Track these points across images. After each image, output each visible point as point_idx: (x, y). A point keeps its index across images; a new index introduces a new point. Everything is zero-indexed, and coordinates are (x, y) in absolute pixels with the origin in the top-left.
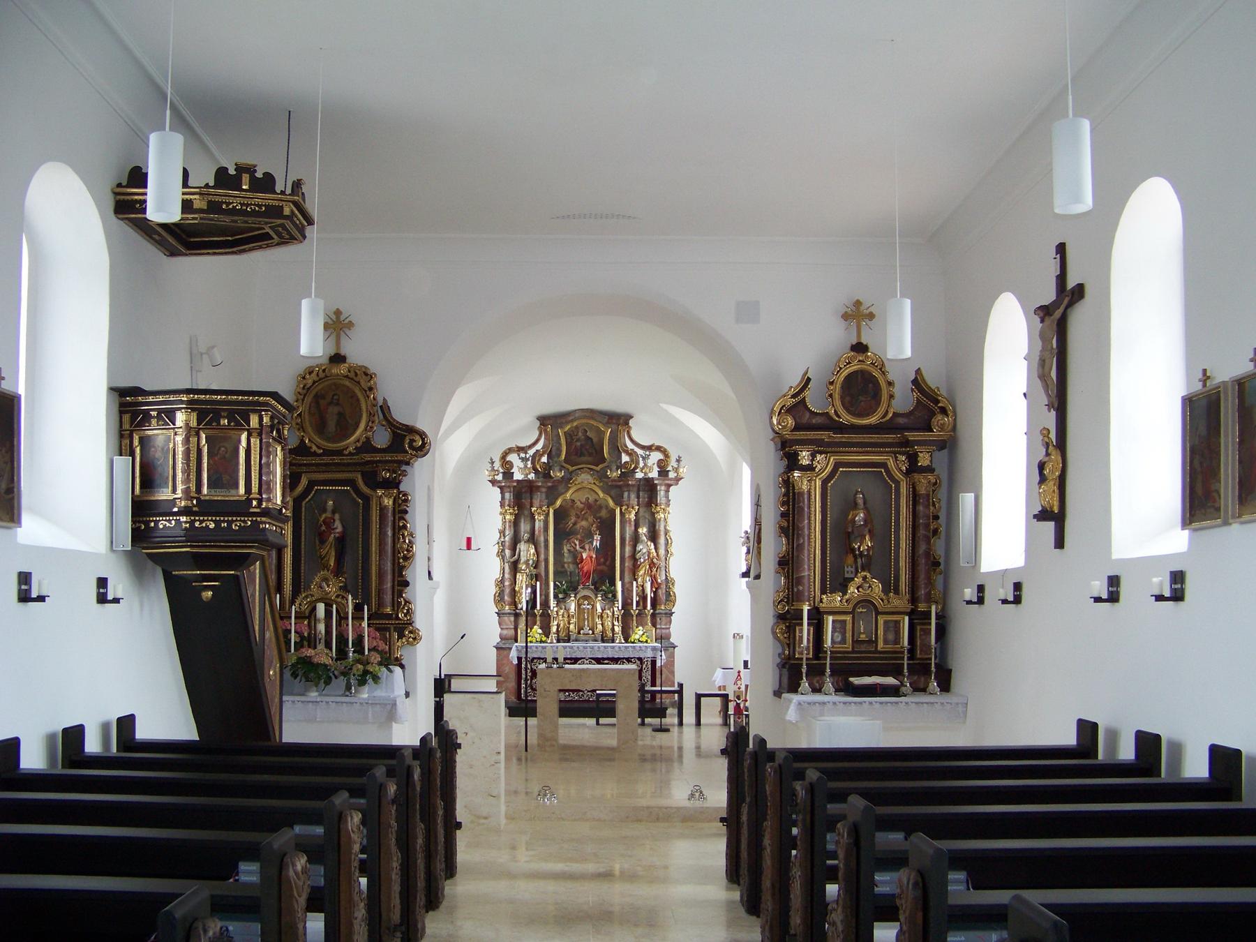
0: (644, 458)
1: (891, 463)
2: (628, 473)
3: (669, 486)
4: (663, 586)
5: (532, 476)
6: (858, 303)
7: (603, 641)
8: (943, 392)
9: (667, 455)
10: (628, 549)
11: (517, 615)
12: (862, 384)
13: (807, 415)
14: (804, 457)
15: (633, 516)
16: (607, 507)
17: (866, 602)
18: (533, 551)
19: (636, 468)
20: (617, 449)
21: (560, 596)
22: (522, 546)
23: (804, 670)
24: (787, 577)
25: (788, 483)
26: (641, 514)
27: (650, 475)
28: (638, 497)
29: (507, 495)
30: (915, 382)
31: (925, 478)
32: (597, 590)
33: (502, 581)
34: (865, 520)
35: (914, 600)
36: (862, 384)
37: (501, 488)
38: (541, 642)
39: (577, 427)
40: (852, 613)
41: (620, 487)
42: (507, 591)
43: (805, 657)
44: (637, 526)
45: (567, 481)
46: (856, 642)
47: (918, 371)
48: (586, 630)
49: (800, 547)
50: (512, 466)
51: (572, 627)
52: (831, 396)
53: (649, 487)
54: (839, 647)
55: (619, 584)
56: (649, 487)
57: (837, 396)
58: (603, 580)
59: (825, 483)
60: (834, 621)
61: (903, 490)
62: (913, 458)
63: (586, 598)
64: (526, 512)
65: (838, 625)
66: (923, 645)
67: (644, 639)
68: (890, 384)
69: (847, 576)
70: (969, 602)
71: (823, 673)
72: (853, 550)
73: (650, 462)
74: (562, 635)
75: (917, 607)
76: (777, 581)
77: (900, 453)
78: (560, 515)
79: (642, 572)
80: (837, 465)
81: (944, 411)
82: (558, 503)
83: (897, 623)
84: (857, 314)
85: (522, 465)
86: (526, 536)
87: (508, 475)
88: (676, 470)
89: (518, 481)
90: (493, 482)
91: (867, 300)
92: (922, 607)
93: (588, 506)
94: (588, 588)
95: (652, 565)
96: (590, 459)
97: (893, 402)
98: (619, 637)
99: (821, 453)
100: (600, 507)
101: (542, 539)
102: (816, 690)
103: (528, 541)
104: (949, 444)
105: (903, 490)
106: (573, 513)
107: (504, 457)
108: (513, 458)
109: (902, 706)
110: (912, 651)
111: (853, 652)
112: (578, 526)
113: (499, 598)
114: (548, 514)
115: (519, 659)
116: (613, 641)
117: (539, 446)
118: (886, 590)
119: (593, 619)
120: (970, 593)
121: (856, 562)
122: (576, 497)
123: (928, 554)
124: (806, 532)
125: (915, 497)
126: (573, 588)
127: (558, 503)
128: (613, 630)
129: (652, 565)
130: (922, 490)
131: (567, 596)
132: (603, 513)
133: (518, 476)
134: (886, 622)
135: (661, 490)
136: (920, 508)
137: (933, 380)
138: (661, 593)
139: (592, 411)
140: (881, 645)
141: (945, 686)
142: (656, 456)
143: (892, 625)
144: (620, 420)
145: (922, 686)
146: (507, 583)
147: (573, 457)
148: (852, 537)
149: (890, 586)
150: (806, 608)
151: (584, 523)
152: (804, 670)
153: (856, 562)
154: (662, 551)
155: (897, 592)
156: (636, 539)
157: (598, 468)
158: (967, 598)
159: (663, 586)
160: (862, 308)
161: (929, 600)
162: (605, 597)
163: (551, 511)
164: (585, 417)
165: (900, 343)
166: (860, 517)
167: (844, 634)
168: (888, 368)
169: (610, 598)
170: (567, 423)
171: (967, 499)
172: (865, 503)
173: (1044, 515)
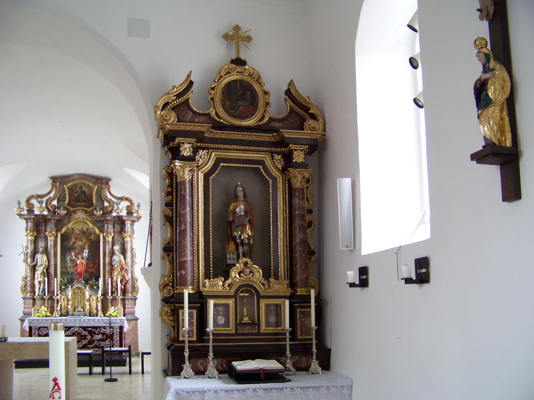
0: (117, 204)
1: (268, 162)
2: (106, 212)
3: (133, 221)
4: (130, 282)
5: (46, 213)
6: (237, 28)
7: (90, 315)
8: (312, 101)
9: (132, 203)
10: (107, 259)
11: (34, 299)
12: (241, 93)
13: (190, 114)
14: (186, 150)
15: (110, 239)
16: (95, 233)
17: (248, 288)
18: (45, 258)
19: (112, 210)
20: (101, 199)
21: (63, 287)
22: (39, 256)
23: (186, 354)
24: (172, 262)
25: (171, 175)
26: (116, 238)
27: (121, 214)
28: (114, 228)
29: (30, 224)
30: (288, 93)
31: (300, 173)
32: (87, 282)
33: (26, 278)
34: (246, 212)
35: (292, 285)
36: (241, 93)
37: (26, 219)
38: (46, 316)
39: (76, 185)
40: (235, 296)
41: (101, 221)
42: (29, 284)
43: (187, 339)
44: (113, 245)
45: (69, 214)
46: (238, 325)
47: (291, 83)
48: (80, 308)
49: (183, 233)
50: (33, 207)
51: (70, 307)
52: (212, 99)
53: (120, 222)
54: (222, 330)
55: (101, 280)
56: (120, 222)
57: (218, 100)
58: (92, 276)
59: (207, 176)
60: (215, 305)
61: (280, 185)
62: (288, 157)
63: (78, 288)
64: (42, 235)
65: (221, 309)
66: (302, 327)
67: (115, 314)
68: (266, 93)
69: (229, 262)
70: (352, 285)
71: (205, 355)
72: (234, 239)
73: (121, 206)
74: (64, 311)
75: (296, 291)
76: (163, 267)
77: (278, 153)
78: (65, 238)
79: (116, 273)
80: (218, 161)
81: (313, 117)
82: (64, 230)
83: (278, 306)
84: (235, 37)
85: (38, 205)
86: (41, 250)
87: (31, 211)
88: (137, 212)
89: (36, 215)
90: (20, 215)
91: (245, 26)
92: (300, 291)
93: (83, 232)
94: (80, 282)
95: (122, 269)
96: (84, 204)
97: (269, 109)
98: (100, 313)
99: (203, 149)
100: (90, 234)
101: (52, 252)
102: (200, 372)
103: (42, 253)
104: (317, 148)
105: (280, 185)
106: (73, 236)
107: (28, 201)
108: (34, 201)
109: (287, 391)
110: (293, 334)
111: (237, 334)
112: (76, 244)
113: (24, 289)
114: (56, 237)
115: (30, 328)
116: (97, 315)
117: (52, 195)
118: (267, 275)
119: (84, 302)
120: (353, 276)
121: (237, 249)
122: (76, 227)
123: (304, 243)
124: (188, 219)
125: (291, 191)
126: (71, 282)
127: (64, 230)
128: (97, 308)
129: (122, 269)
130: (297, 183)
131: (67, 287)
132: (93, 237)
133: (37, 212)
134: (267, 306)
135: (128, 224)
136: (296, 201)
137: (303, 89)
138: (129, 286)
139: (85, 175)
140: (263, 327)
141: (326, 365)
142: (124, 204)
143: (273, 308)
144: (103, 182)
145: (303, 366)
146: (28, 279)
147: (73, 203)
148: (233, 226)
149: (268, 274)
150: (187, 292)
151: (80, 243)
152: (186, 354)
153: (237, 249)
154: (129, 260)
155: (277, 278)
156: (112, 253)
157: (89, 210)
158: (351, 281)
159: (130, 282)
160: (240, 32)
161: (307, 285)
162: (92, 287)
163: (59, 235)
164: (80, 178)
165: (274, 69)
166: (241, 209)
167: (227, 317)
168: (263, 80)
169: (94, 288)
170: (70, 181)
171: (346, 183)
172: (245, 196)
173: (489, 154)
